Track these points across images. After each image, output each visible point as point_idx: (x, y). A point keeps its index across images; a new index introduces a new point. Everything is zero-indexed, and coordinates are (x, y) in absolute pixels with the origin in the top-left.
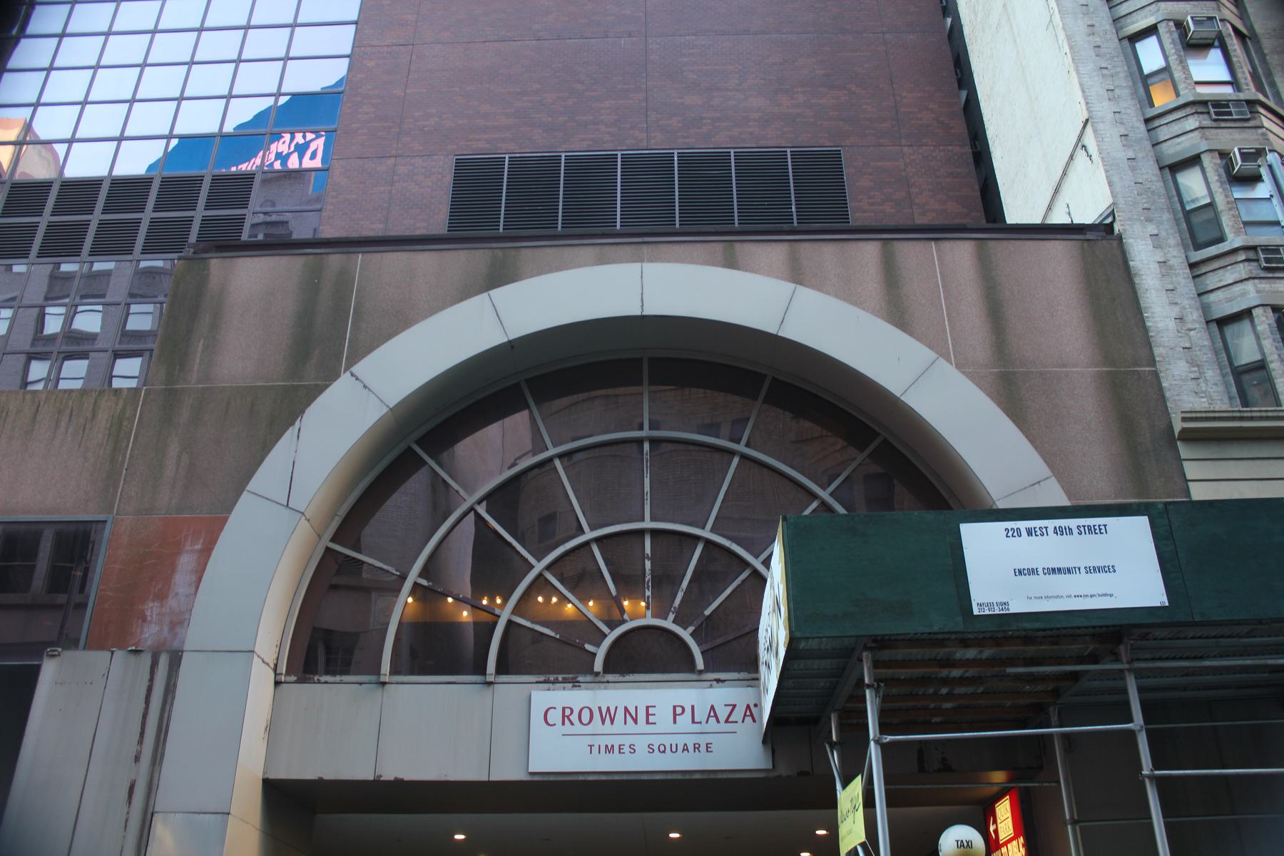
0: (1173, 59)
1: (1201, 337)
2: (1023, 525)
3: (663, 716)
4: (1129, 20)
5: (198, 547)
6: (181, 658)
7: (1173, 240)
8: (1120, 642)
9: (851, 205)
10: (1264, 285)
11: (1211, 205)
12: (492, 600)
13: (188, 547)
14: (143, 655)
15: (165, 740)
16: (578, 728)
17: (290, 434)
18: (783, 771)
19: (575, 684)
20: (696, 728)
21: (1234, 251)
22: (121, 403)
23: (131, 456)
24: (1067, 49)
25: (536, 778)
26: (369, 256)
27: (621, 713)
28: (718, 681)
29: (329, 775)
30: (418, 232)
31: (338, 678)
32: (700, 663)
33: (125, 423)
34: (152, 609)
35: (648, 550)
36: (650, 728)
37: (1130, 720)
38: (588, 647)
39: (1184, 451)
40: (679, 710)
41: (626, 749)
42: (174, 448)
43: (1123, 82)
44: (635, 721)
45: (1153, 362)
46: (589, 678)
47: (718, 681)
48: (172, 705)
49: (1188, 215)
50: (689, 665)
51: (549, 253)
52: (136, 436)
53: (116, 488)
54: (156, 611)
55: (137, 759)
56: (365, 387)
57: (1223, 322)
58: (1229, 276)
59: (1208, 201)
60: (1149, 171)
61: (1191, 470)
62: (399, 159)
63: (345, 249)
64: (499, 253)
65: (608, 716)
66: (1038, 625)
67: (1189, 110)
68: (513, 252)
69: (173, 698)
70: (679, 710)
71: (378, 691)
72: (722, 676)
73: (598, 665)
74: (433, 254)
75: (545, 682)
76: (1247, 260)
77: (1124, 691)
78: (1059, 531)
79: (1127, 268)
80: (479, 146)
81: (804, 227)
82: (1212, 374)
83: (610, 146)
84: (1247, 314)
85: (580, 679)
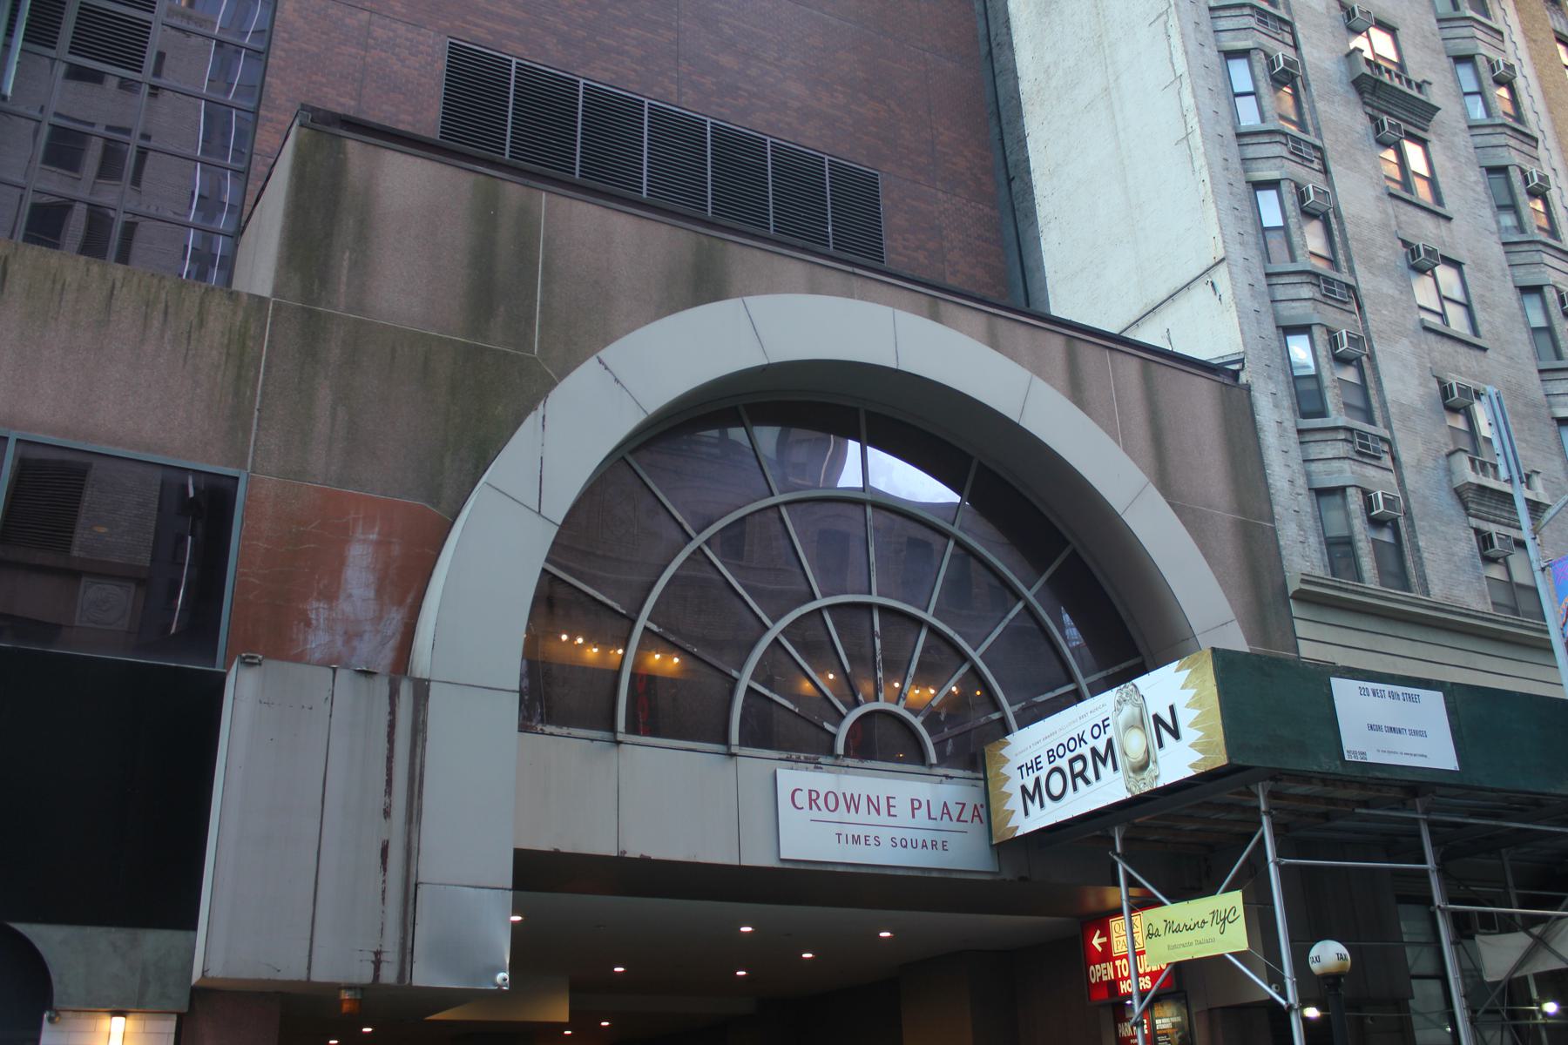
0: (1292, 221)
1: (1306, 502)
2: (1371, 685)
3: (902, 808)
4: (1260, 164)
5: (373, 537)
6: (428, 689)
7: (1286, 403)
8: (1416, 795)
9: (886, 242)
10: (1356, 467)
11: (1317, 378)
12: (572, 638)
13: (359, 535)
14: (376, 678)
15: (420, 792)
16: (825, 814)
17: (531, 421)
18: (1008, 875)
19: (818, 766)
20: (931, 824)
21: (1336, 429)
22: (241, 314)
23: (264, 393)
24: (1205, 175)
25: (787, 866)
26: (556, 198)
27: (864, 801)
28: (947, 777)
29: (566, 847)
30: (401, 127)
31: (565, 731)
32: (933, 757)
33: (250, 343)
34: (318, 610)
35: (877, 628)
36: (891, 821)
37: (1424, 862)
38: (828, 726)
39: (1296, 610)
40: (916, 804)
41: (872, 841)
42: (324, 396)
43: (1250, 229)
44: (878, 811)
45: (1272, 520)
46: (829, 760)
47: (947, 777)
48: (424, 748)
49: (1296, 378)
50: (921, 758)
51: (793, 268)
52: (268, 367)
53: (247, 432)
54: (323, 614)
55: (387, 813)
56: (617, 380)
57: (1321, 493)
58: (1330, 451)
59: (1312, 371)
60: (1270, 329)
61: (1301, 628)
62: (375, 17)
63: (526, 181)
64: (705, 240)
65: (852, 803)
66: (1385, 775)
67: (1304, 278)
68: (720, 244)
69: (425, 740)
70: (916, 804)
71: (613, 751)
72: (950, 772)
73: (840, 748)
74: (631, 219)
75: (787, 760)
76: (1345, 440)
77: (1419, 836)
78: (1392, 695)
79: (1254, 421)
80: (480, 34)
81: (780, 237)
82: (1313, 540)
83: (635, 88)
84: (1342, 490)
85: (821, 760)
